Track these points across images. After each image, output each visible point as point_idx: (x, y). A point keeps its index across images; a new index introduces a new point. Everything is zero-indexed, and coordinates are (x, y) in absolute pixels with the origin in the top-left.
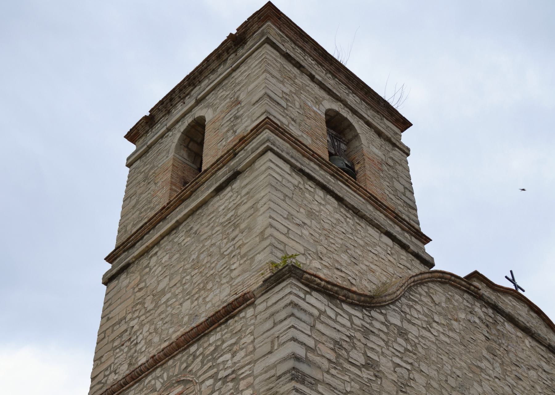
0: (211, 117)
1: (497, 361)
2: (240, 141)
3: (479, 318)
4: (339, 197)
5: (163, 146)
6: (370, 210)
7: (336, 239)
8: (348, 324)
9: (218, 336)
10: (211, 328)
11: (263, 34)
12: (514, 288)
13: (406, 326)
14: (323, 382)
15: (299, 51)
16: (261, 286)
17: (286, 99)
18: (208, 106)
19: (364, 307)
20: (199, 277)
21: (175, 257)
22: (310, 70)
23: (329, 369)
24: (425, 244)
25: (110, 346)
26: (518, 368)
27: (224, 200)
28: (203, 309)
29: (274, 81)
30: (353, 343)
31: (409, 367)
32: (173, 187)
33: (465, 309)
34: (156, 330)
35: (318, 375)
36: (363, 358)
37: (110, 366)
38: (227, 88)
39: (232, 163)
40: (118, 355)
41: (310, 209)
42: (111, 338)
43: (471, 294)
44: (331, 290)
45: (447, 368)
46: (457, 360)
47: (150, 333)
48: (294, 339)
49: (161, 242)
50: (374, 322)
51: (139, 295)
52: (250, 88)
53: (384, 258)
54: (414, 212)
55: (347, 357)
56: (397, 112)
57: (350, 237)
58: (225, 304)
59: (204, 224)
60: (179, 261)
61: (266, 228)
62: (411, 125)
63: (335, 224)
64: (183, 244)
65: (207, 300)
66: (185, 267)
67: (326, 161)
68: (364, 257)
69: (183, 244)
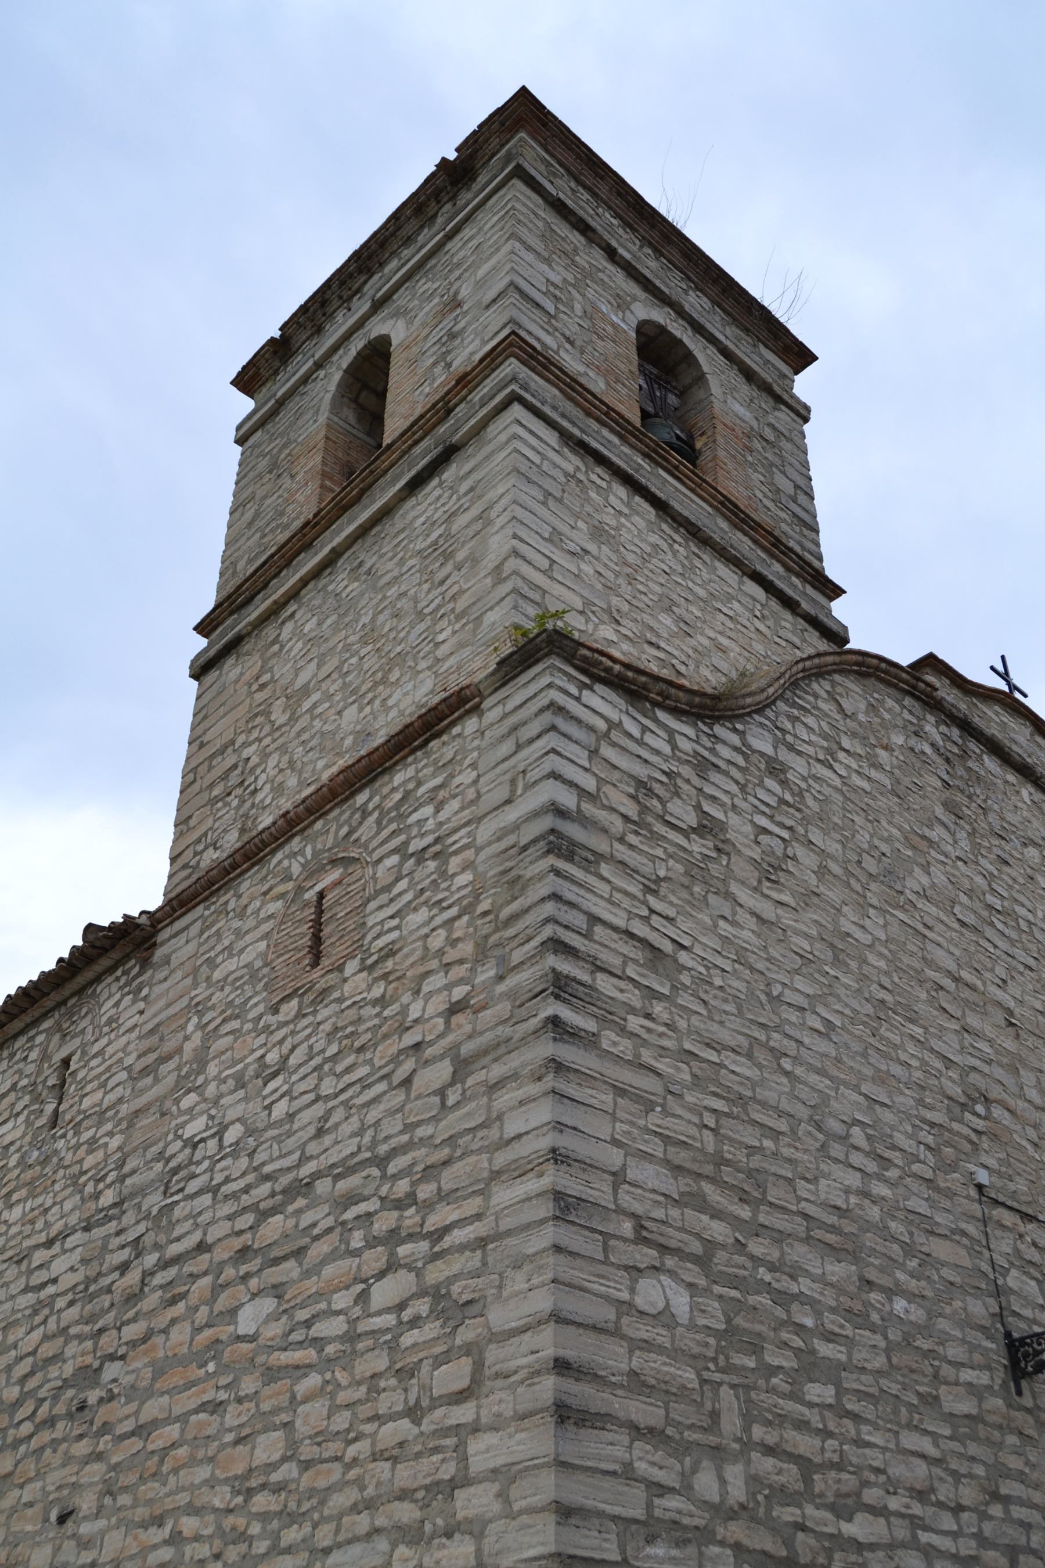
0: (402, 336)
1: (963, 828)
2: (458, 382)
3: (932, 745)
4: (659, 499)
5: (307, 399)
6: (722, 529)
7: (650, 584)
8: (667, 749)
9: (410, 772)
10: (397, 757)
11: (509, 157)
12: (1006, 689)
13: (784, 755)
14: (610, 859)
15: (586, 196)
16: (493, 674)
17: (555, 296)
18: (396, 315)
19: (700, 717)
20: (374, 660)
21: (329, 621)
22: (606, 236)
23: (624, 834)
24: (832, 599)
25: (205, 796)
26: (1003, 842)
27: (425, 504)
28: (381, 720)
29: (530, 257)
30: (675, 785)
31: (785, 834)
32: (327, 483)
33: (904, 727)
34: (291, 764)
35: (602, 845)
36: (694, 814)
37: (205, 834)
38: (434, 275)
39: (441, 429)
40: (220, 814)
41: (597, 523)
42: (207, 781)
43: (917, 698)
44: (633, 682)
45: (863, 838)
46: (884, 823)
47: (281, 771)
48: (555, 775)
49: (303, 592)
50: (719, 747)
51: (260, 697)
52: (481, 273)
53: (748, 624)
54: (813, 535)
55: (661, 813)
56: (787, 331)
57: (680, 580)
58: (424, 711)
59: (385, 554)
60: (336, 628)
61: (505, 559)
62: (816, 358)
63: (649, 555)
64: (344, 595)
65: (390, 703)
66: (349, 641)
67: (634, 427)
68: (705, 622)
69: (344, 595)
